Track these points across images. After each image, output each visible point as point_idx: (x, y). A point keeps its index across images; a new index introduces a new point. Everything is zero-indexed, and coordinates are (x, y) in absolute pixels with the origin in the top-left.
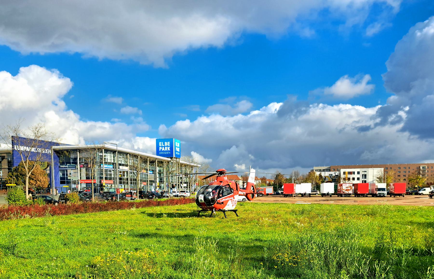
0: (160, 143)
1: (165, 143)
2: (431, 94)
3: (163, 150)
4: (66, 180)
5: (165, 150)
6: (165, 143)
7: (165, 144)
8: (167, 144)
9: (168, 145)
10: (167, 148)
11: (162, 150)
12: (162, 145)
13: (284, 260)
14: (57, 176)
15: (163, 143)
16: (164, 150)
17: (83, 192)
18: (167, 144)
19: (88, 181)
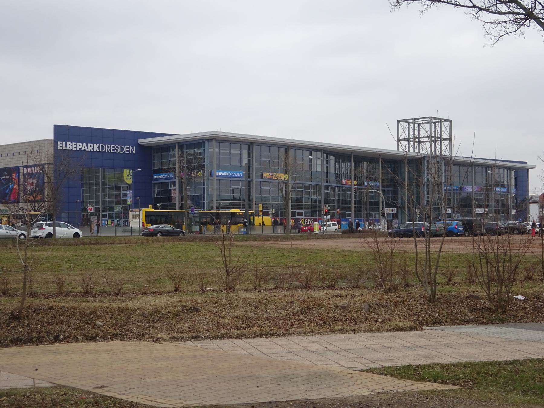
0: (59, 143)
1: (68, 143)
2: (2, 211)
3: (85, 150)
4: (313, 191)
5: (89, 150)
6: (68, 143)
7: (68, 146)
8: (72, 146)
9: (73, 149)
10: (92, 147)
11: (82, 149)
12: (62, 147)
13: (233, 298)
14: (436, 2)
15: (64, 143)
16: (87, 150)
17: (475, 340)
18: (72, 146)
19: (162, 176)
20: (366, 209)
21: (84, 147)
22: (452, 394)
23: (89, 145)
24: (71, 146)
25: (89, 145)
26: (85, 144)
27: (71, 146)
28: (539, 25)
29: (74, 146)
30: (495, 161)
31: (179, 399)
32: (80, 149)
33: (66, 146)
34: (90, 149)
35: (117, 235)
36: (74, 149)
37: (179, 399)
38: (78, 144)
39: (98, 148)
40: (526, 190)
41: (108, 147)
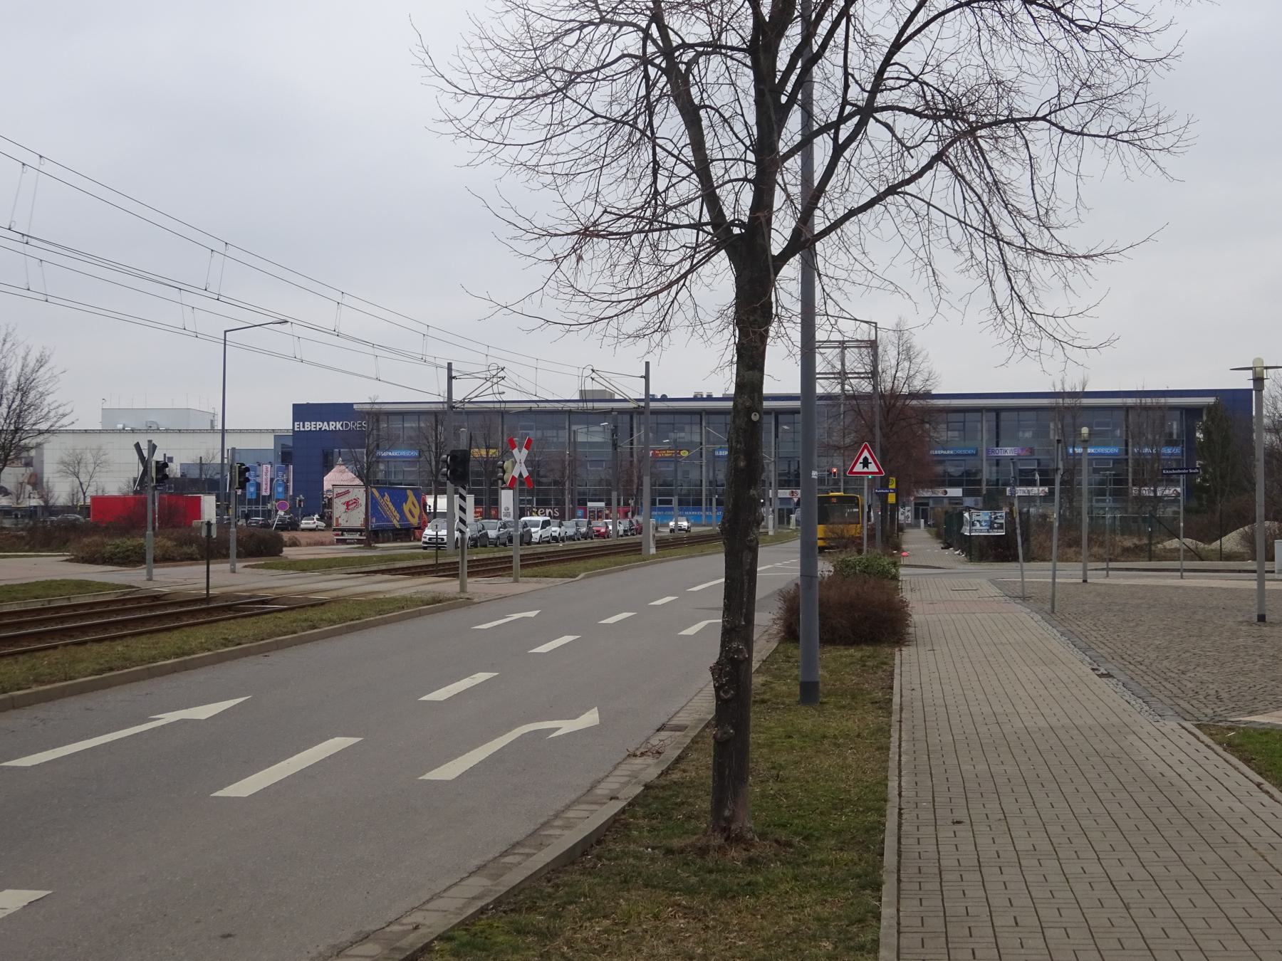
1: (306, 423)
6: (306, 423)
7: (306, 426)
20: (1121, 656)
21: (325, 426)
22: (369, 613)
23: (331, 423)
24: (309, 426)
25: (331, 423)
26: (326, 423)
27: (309, 426)
28: (829, 31)
29: (313, 426)
30: (671, 417)
31: (658, 730)
32: (320, 429)
33: (304, 427)
34: (332, 428)
35: (439, 562)
36: (313, 429)
37: (658, 730)
38: (318, 423)
39: (342, 426)
40: (452, 399)
41: (354, 424)
